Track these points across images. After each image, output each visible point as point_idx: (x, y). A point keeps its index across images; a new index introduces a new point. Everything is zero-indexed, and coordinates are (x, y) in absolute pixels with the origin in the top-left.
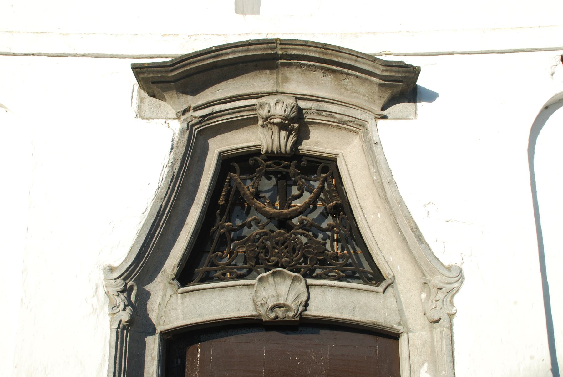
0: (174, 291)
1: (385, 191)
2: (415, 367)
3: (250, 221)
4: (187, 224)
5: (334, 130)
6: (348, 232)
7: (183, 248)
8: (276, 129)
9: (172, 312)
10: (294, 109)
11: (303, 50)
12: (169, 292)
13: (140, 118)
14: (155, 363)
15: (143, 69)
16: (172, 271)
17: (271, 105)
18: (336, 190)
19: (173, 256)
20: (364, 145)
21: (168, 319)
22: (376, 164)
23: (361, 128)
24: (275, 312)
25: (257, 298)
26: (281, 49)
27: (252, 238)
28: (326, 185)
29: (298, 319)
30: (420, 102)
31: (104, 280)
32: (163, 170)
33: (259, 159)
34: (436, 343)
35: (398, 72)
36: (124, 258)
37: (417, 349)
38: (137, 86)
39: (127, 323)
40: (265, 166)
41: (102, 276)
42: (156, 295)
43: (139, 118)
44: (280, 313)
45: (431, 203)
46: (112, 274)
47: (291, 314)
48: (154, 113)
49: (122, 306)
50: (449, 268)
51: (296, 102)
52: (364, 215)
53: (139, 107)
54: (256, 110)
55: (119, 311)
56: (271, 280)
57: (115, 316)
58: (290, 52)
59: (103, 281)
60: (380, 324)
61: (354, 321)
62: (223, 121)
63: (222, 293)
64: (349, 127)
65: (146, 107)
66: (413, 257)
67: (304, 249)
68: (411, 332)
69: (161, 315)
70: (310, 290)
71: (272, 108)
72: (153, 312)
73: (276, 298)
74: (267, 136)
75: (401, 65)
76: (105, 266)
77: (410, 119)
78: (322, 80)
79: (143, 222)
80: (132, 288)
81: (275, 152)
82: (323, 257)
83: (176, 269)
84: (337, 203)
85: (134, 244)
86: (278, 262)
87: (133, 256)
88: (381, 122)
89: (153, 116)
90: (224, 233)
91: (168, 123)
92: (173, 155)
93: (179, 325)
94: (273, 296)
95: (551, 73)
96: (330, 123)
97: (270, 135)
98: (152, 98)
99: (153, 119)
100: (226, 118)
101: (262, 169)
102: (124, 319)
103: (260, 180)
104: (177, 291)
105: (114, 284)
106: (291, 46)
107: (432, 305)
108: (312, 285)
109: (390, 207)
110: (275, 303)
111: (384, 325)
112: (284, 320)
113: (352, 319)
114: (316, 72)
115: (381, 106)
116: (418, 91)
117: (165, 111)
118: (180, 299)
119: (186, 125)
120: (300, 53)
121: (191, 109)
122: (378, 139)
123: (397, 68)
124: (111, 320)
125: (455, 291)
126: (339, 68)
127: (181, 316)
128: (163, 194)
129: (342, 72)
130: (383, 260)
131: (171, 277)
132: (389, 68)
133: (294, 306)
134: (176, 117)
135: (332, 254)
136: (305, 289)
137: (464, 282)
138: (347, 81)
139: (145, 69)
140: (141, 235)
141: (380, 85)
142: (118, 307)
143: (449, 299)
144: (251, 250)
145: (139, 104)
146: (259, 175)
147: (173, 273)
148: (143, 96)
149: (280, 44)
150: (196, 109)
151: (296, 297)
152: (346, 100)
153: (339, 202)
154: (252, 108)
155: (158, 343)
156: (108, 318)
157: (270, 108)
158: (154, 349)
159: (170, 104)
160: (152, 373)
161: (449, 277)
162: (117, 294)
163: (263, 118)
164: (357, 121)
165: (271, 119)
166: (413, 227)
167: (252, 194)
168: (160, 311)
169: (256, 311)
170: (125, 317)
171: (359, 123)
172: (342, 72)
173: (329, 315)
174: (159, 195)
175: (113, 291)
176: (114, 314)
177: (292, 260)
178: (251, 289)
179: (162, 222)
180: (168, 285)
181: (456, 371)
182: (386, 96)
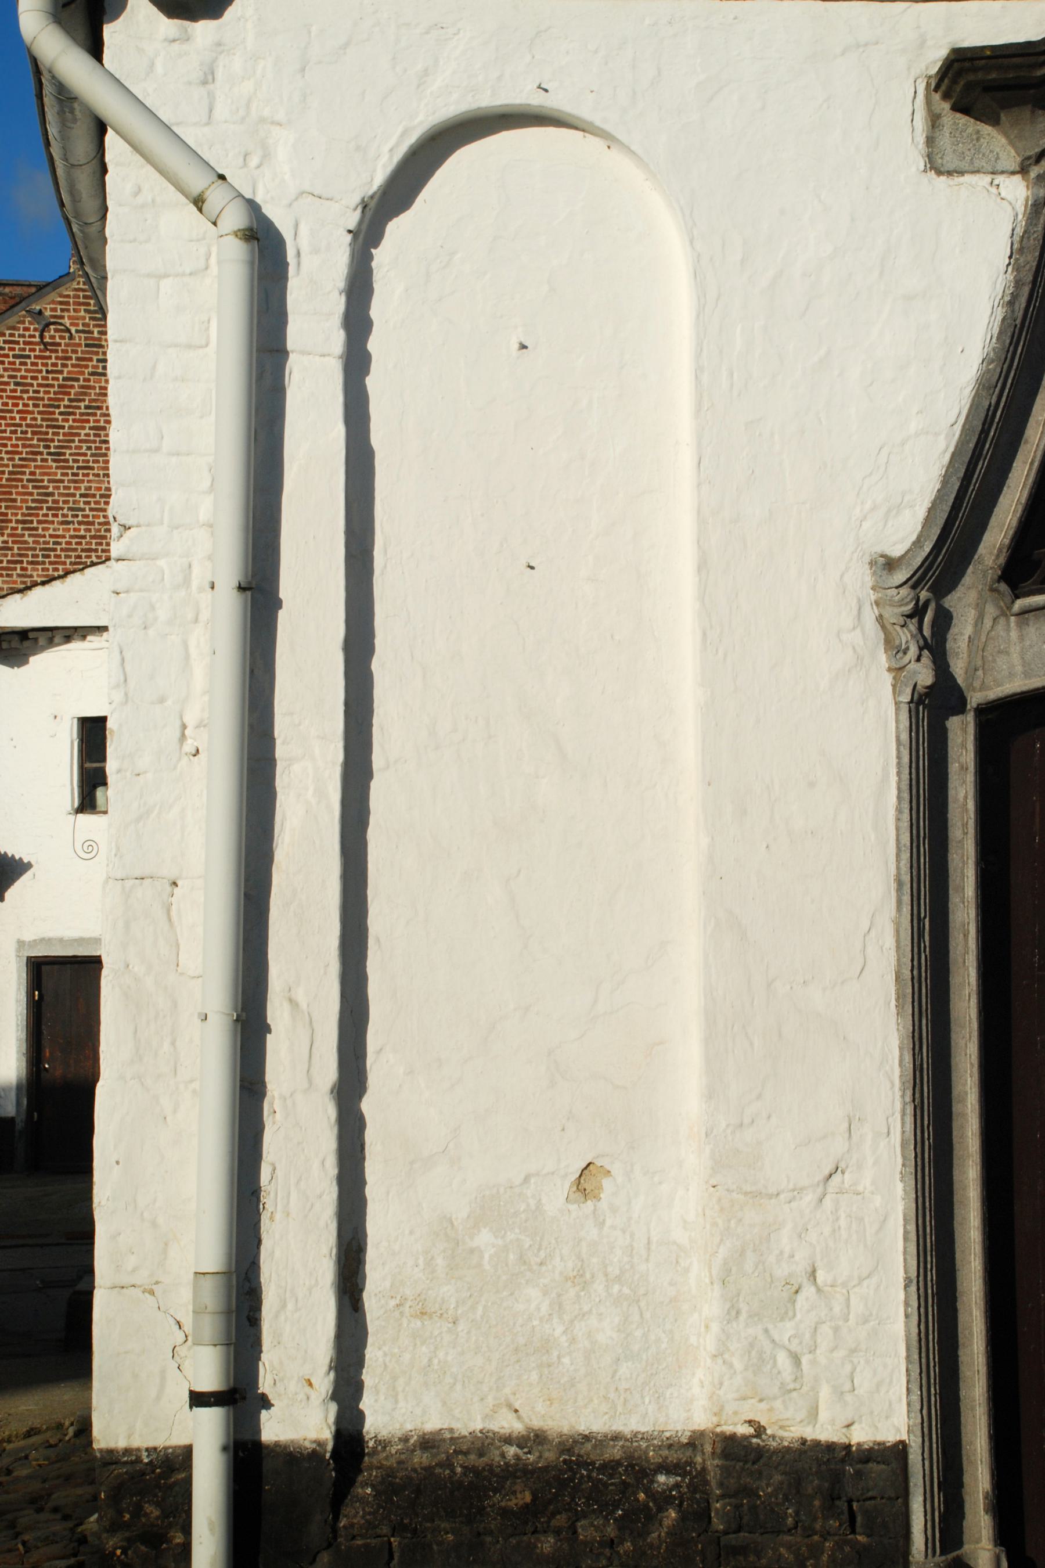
0: (1001, 608)
4: (1026, 442)
7: (1021, 503)
9: (998, 659)
13: (933, 172)
14: (970, 778)
15: (978, 62)
16: (994, 561)
19: (996, 524)
21: (991, 676)
31: (873, 588)
32: (992, 313)
36: (914, 537)
38: (923, 81)
39: (927, 690)
41: (869, 580)
42: (963, 618)
43: (931, 171)
46: (891, 574)
48: (964, 158)
53: (930, 141)
55: (910, 662)
57: (903, 674)
59: (872, 592)
65: (945, 141)
69: (975, 665)
72: (958, 659)
79: (952, 449)
83: (1005, 554)
87: (933, 531)
89: (964, 165)
91: (998, 183)
92: (1012, 272)
99: (963, 175)
102: (922, 681)
104: (1009, 608)
105: (896, 598)
117: (991, 151)
118: (1015, 627)
124: (893, 683)
127: (1019, 669)
128: (993, 375)
131: (993, 574)
139: (983, 62)
140: (948, 480)
142: (905, 653)
145: (927, 131)
147: (998, 564)
148: (938, 111)
155: (973, 732)
156: (888, 679)
158: (963, 745)
159: (1006, 135)
160: (962, 800)
162: (903, 623)
168: (971, 656)
170: (924, 675)
174: (984, 378)
175: (893, 615)
179: (987, 446)
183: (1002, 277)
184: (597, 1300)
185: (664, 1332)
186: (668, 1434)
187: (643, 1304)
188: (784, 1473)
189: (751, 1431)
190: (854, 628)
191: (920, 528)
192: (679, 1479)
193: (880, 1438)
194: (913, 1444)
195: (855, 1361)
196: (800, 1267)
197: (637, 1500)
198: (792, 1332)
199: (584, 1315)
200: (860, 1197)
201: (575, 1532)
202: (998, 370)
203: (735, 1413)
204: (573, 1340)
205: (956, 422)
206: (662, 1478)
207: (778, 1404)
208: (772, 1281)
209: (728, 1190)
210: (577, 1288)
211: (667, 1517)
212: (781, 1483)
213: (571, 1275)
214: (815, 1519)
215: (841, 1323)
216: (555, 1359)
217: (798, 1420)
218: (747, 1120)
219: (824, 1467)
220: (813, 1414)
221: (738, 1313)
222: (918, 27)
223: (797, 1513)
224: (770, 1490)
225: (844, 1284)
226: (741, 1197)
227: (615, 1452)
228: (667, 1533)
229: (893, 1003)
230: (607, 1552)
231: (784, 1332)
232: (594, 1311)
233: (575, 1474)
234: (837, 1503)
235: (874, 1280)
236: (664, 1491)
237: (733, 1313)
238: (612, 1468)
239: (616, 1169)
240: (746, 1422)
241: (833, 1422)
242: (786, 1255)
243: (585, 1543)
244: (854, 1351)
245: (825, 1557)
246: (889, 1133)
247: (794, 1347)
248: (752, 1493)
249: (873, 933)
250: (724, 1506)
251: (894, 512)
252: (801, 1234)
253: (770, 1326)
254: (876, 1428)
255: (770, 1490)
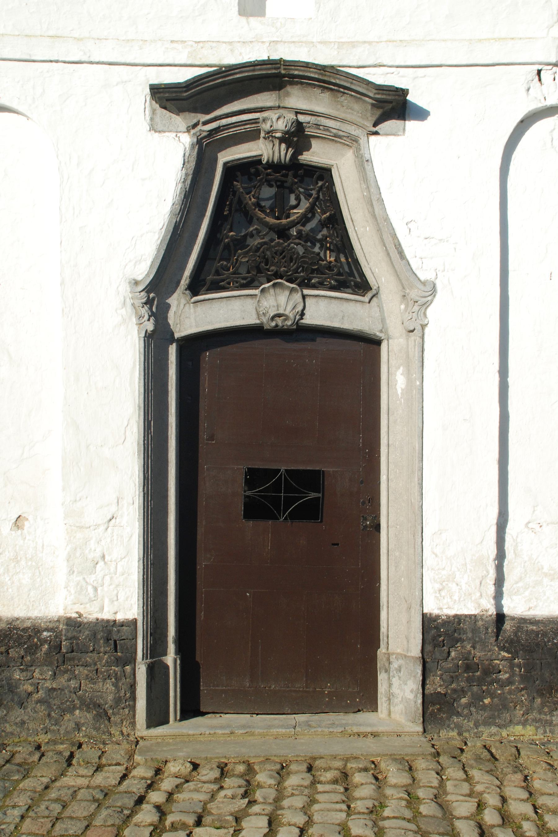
1: (373, 208)
2: (392, 370)
3: (252, 231)
5: (330, 143)
6: (339, 242)
8: (277, 142)
10: (294, 124)
11: (304, 71)
12: (183, 301)
17: (273, 120)
18: (330, 199)
20: (357, 160)
22: (367, 181)
23: (354, 143)
24: (275, 321)
25: (260, 308)
26: (285, 69)
27: (253, 248)
28: (321, 194)
29: (295, 327)
30: (409, 120)
33: (260, 167)
34: (410, 350)
35: (389, 95)
36: (146, 273)
37: (395, 354)
40: (265, 175)
41: (129, 289)
44: (279, 321)
45: (413, 221)
47: (289, 323)
49: (146, 317)
50: (424, 283)
51: (296, 116)
52: (355, 228)
53: (152, 119)
54: (259, 123)
55: (145, 321)
56: (272, 291)
58: (292, 72)
60: (365, 332)
61: (343, 329)
62: (228, 134)
63: (229, 302)
64: (343, 141)
65: (157, 119)
66: (396, 271)
67: (301, 259)
68: (391, 338)
70: (306, 300)
71: (274, 123)
73: (276, 308)
74: (268, 147)
75: (392, 89)
76: (131, 280)
77: (398, 135)
78: (320, 96)
79: (161, 238)
80: (153, 299)
81: (276, 163)
82: (316, 267)
84: (330, 215)
85: (154, 259)
86: (277, 272)
88: (372, 138)
89: (165, 129)
90: (228, 243)
93: (193, 332)
94: (274, 306)
95: (526, 88)
96: (326, 137)
97: (271, 147)
98: (163, 110)
100: (231, 131)
101: (262, 179)
103: (261, 190)
104: (190, 301)
106: (293, 67)
107: (409, 316)
108: (307, 295)
109: (378, 223)
110: (276, 313)
111: (368, 332)
112: (283, 328)
113: (342, 327)
114: (315, 89)
115: (373, 122)
116: (407, 105)
119: (195, 140)
120: (301, 73)
121: (200, 123)
122: (369, 156)
123: (388, 92)
125: (428, 304)
126: (336, 88)
127: (194, 324)
129: (339, 91)
130: (370, 271)
132: (381, 92)
133: (291, 316)
134: (186, 131)
135: (325, 264)
136: (301, 300)
137: (436, 296)
138: (343, 98)
139: (161, 90)
141: (373, 105)
142: (143, 318)
143: (423, 311)
144: (253, 260)
146: (260, 185)
148: (155, 108)
149: (284, 65)
150: (205, 123)
151: (293, 307)
152: (342, 115)
153: (333, 212)
154: (255, 121)
156: (136, 328)
157: (273, 123)
159: (181, 118)
161: (424, 291)
163: (265, 132)
164: (351, 137)
165: (272, 133)
166: (397, 244)
167: (254, 204)
169: (259, 320)
170: (150, 326)
171: (353, 139)
172: (339, 91)
173: (321, 324)
175: (138, 303)
176: (141, 324)
177: (290, 269)
178: (254, 299)
180: (181, 295)
181: (424, 374)
182: (378, 112)
183: (180, 172)
184: (22, 567)
185: (48, 579)
186: (49, 617)
187: (40, 569)
188: (90, 631)
189: (77, 616)
190: (122, 308)
191: (148, 269)
192: (52, 633)
193: (127, 617)
194: (139, 619)
195: (119, 589)
196: (98, 554)
197: (33, 641)
198: (94, 579)
199: (17, 573)
200: (122, 528)
201: (8, 654)
202: (179, 208)
203: (71, 609)
204: (13, 583)
205: (162, 228)
206: (45, 633)
207: (88, 605)
208: (87, 560)
209: (70, 526)
210: (15, 563)
211: (44, 648)
212: (88, 634)
213: (12, 558)
214: (101, 647)
215: (113, 575)
216: (6, 590)
217: (96, 611)
218: (78, 499)
219: (105, 628)
220: (102, 609)
221: (73, 572)
222: (146, 76)
223: (94, 645)
224: (83, 637)
225: (115, 561)
226: (75, 528)
227: (28, 624)
228: (44, 653)
229: (136, 453)
230: (20, 660)
231: (91, 579)
232: (21, 572)
233: (12, 632)
234: (110, 641)
235: (126, 559)
236: (45, 638)
237: (71, 572)
238: (27, 630)
239: (30, 518)
240: (75, 612)
241: (109, 612)
242: (93, 550)
243: (12, 658)
244: (118, 586)
245: (104, 661)
246: (133, 503)
247: (95, 584)
248: (77, 638)
249: (129, 427)
250: (66, 643)
251: (138, 263)
252: (99, 542)
253: (86, 577)
254: (126, 614)
255: (83, 637)
